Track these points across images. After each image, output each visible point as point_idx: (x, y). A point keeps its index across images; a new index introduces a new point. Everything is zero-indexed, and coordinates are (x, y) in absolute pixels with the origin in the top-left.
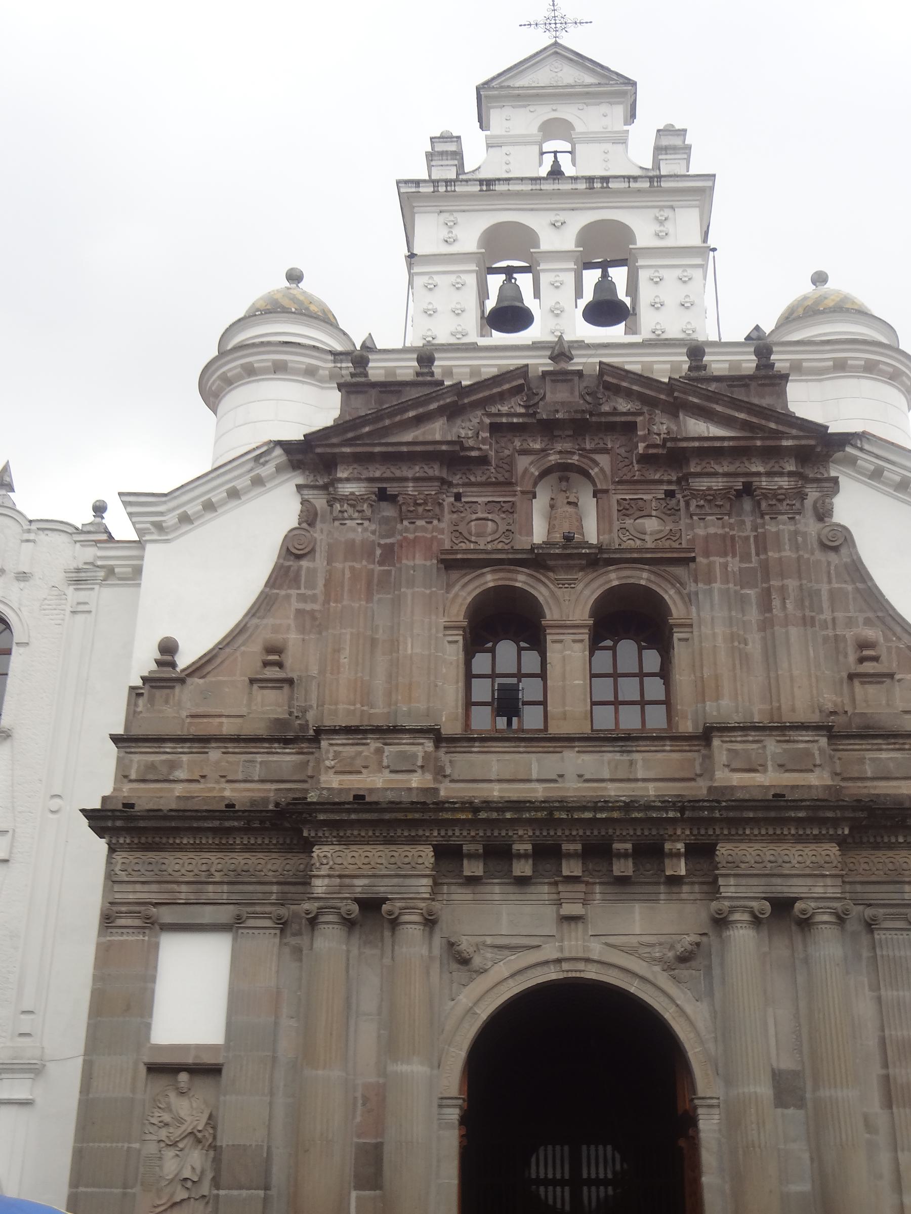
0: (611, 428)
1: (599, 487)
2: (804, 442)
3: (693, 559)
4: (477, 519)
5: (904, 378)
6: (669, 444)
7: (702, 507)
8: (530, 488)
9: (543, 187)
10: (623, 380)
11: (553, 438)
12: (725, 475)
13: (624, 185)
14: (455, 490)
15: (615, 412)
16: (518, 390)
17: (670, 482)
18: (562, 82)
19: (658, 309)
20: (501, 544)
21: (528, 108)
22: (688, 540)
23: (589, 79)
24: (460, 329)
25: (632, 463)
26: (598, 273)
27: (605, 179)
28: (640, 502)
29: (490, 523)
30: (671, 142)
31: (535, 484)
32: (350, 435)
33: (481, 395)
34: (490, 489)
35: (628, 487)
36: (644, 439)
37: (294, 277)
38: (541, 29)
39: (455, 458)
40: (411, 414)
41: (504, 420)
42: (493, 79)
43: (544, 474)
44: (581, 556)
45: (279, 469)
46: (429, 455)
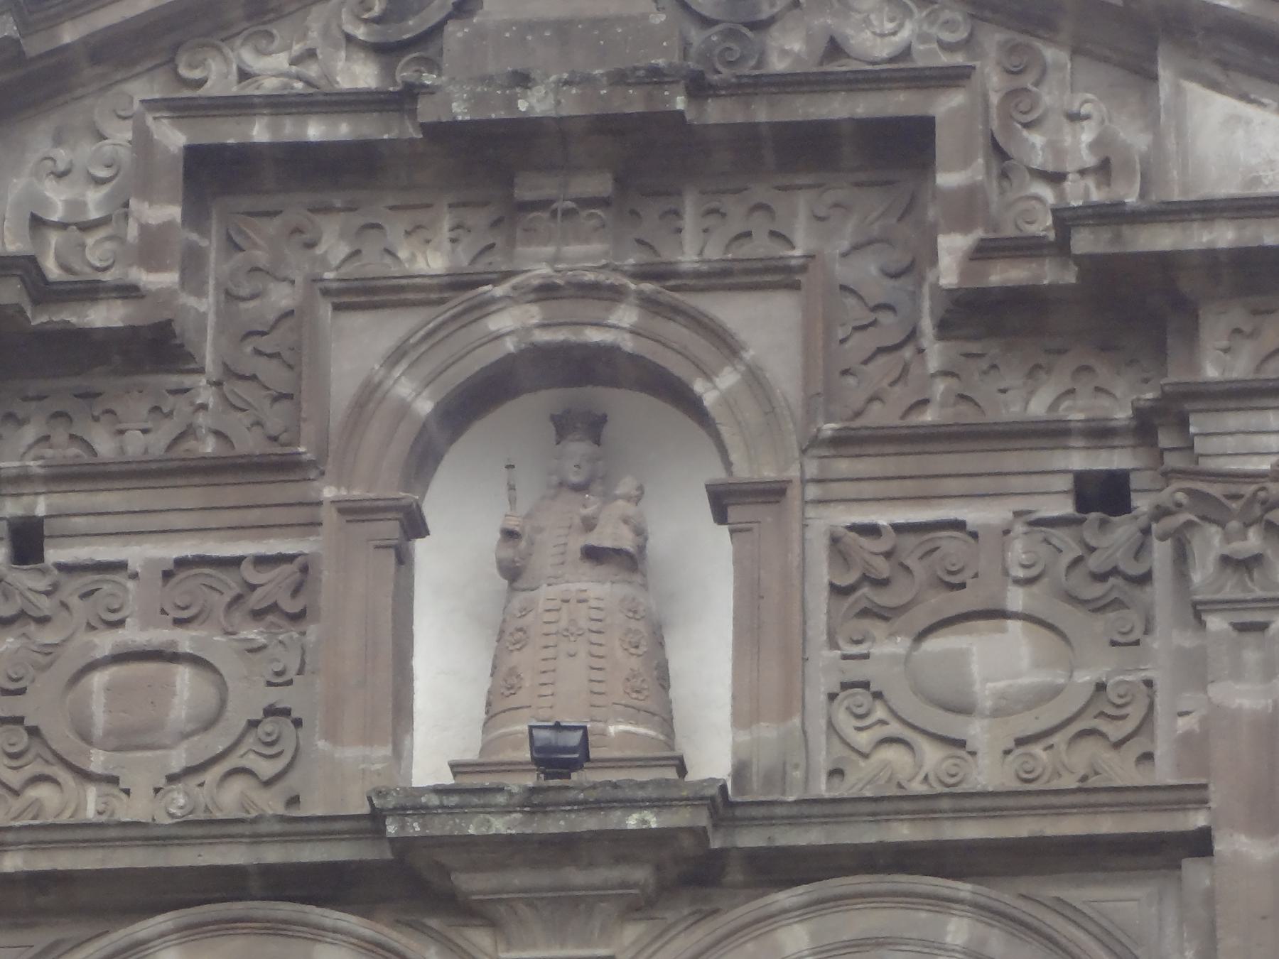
0: (809, 150)
1: (743, 471)
3: (1201, 843)
4: (123, 657)
6: (1084, 242)
7: (1246, 565)
8: (388, 488)
11: (514, 215)
17: (1100, 434)
20: (238, 786)
22: (1186, 740)
25: (913, 335)
28: (950, 543)
29: (183, 675)
31: (423, 460)
34: (190, 496)
35: (890, 465)
36: (967, 207)
41: (259, 132)
44: (625, 846)
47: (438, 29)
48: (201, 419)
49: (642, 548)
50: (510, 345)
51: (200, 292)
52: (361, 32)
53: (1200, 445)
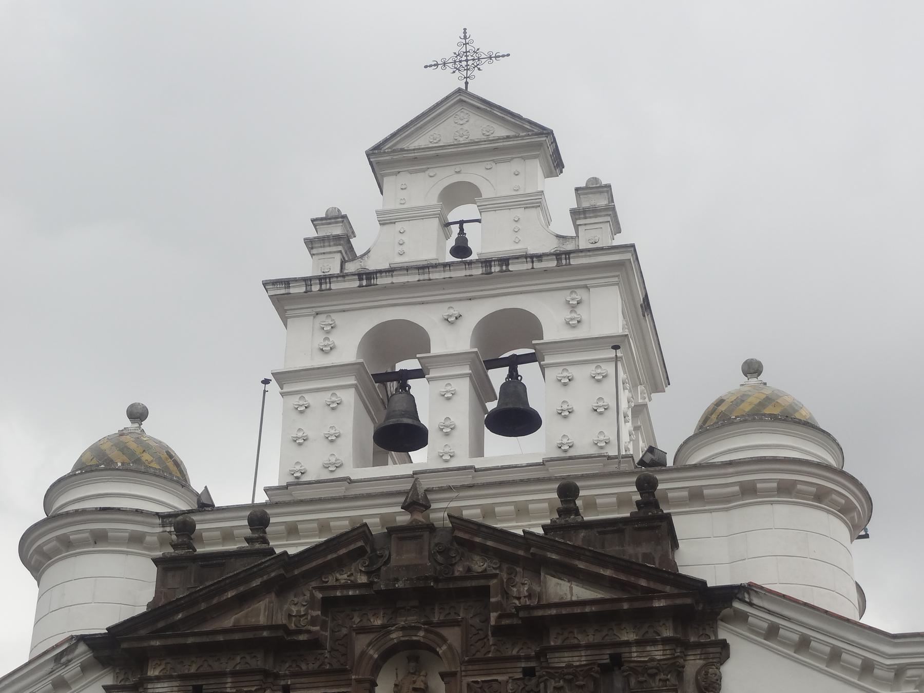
0: (463, 594)
2: (679, 601)
5: (834, 497)
6: (522, 614)
9: (432, 276)
10: (476, 535)
12: (588, 647)
13: (526, 266)
14: (283, 683)
15: (469, 574)
16: (359, 553)
17: (528, 658)
18: (470, 135)
19: (565, 417)
21: (427, 172)
23: (500, 131)
24: (333, 460)
25: (487, 636)
26: (505, 371)
27: (504, 261)
28: (495, 685)
30: (595, 203)
31: (376, 668)
32: (161, 624)
33: (314, 564)
37: (137, 414)
38: (449, 70)
39: (281, 644)
40: (230, 594)
42: (386, 141)
43: (387, 655)
45: (85, 668)
46: (250, 642)
47: (379, 569)
48: (326, 660)
49: (427, 687)
50: (395, 641)
51: (326, 631)
52: (363, 569)
53: (550, 661)
